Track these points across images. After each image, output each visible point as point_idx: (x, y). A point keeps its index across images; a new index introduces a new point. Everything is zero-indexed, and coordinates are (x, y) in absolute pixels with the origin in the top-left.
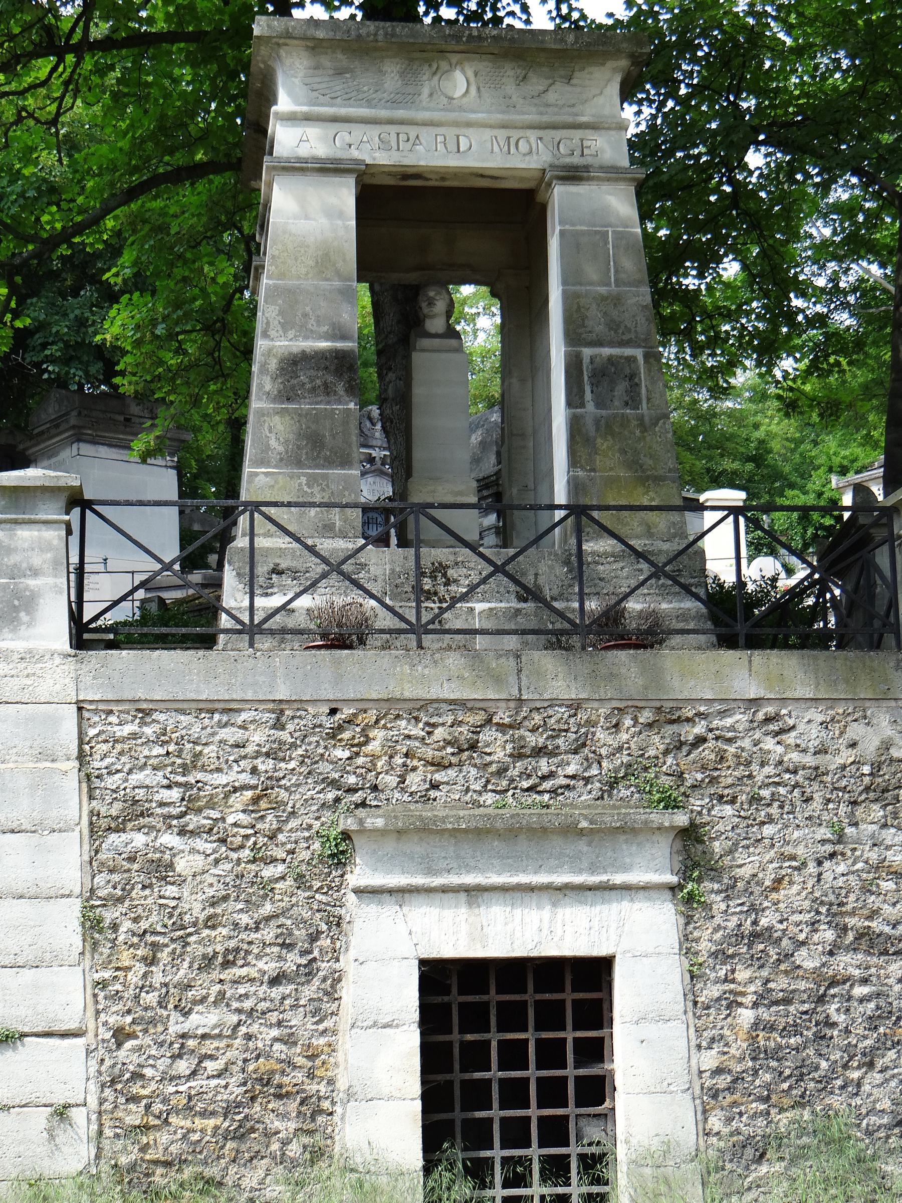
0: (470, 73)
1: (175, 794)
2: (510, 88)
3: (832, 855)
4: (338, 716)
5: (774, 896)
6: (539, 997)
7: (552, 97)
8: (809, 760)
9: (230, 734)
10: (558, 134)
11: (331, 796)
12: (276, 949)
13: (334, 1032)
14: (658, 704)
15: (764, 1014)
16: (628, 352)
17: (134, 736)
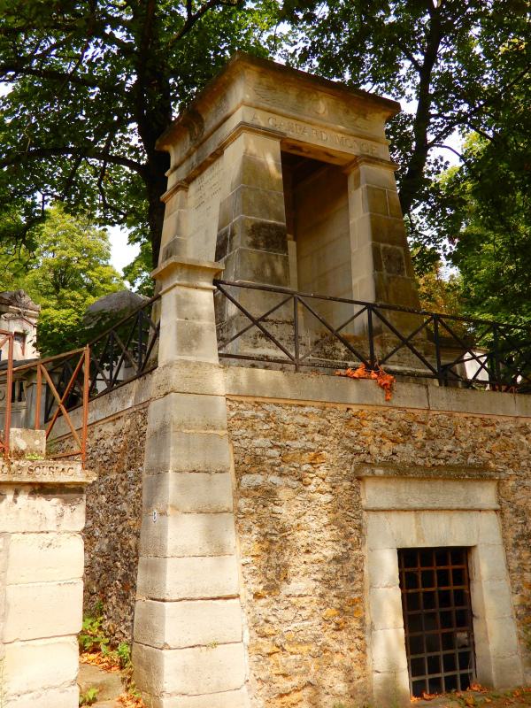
1: (275, 452)
2: (341, 113)
4: (350, 412)
7: (358, 123)
9: (302, 420)
10: (363, 141)
11: (350, 456)
12: (330, 543)
14: (481, 416)
17: (254, 417)
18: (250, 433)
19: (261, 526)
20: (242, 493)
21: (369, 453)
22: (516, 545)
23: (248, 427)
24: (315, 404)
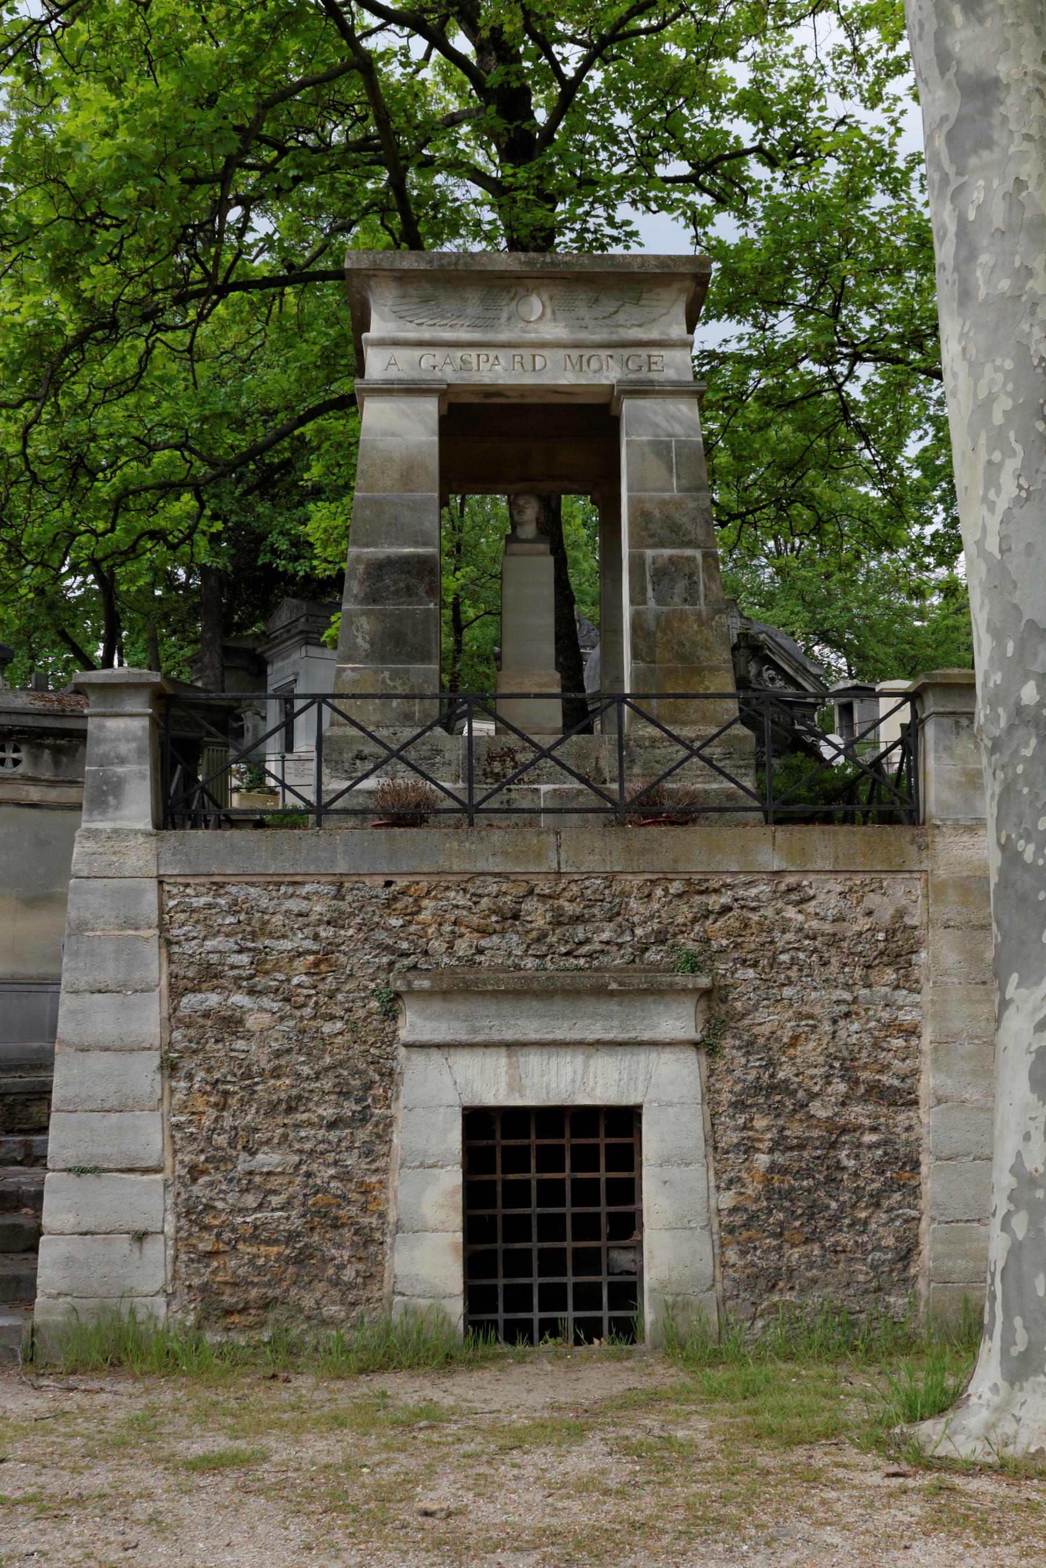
0: (546, 297)
1: (244, 959)
2: (583, 311)
3: (847, 1015)
5: (791, 1051)
6: (575, 1141)
8: (827, 927)
10: (626, 352)
13: (385, 1171)
15: (780, 1158)
16: (688, 552)
17: (210, 906)
18: (200, 930)
19: (209, 1070)
20: (180, 1020)
21: (426, 953)
22: (739, 1106)
23: (197, 922)
24: (323, 879)
